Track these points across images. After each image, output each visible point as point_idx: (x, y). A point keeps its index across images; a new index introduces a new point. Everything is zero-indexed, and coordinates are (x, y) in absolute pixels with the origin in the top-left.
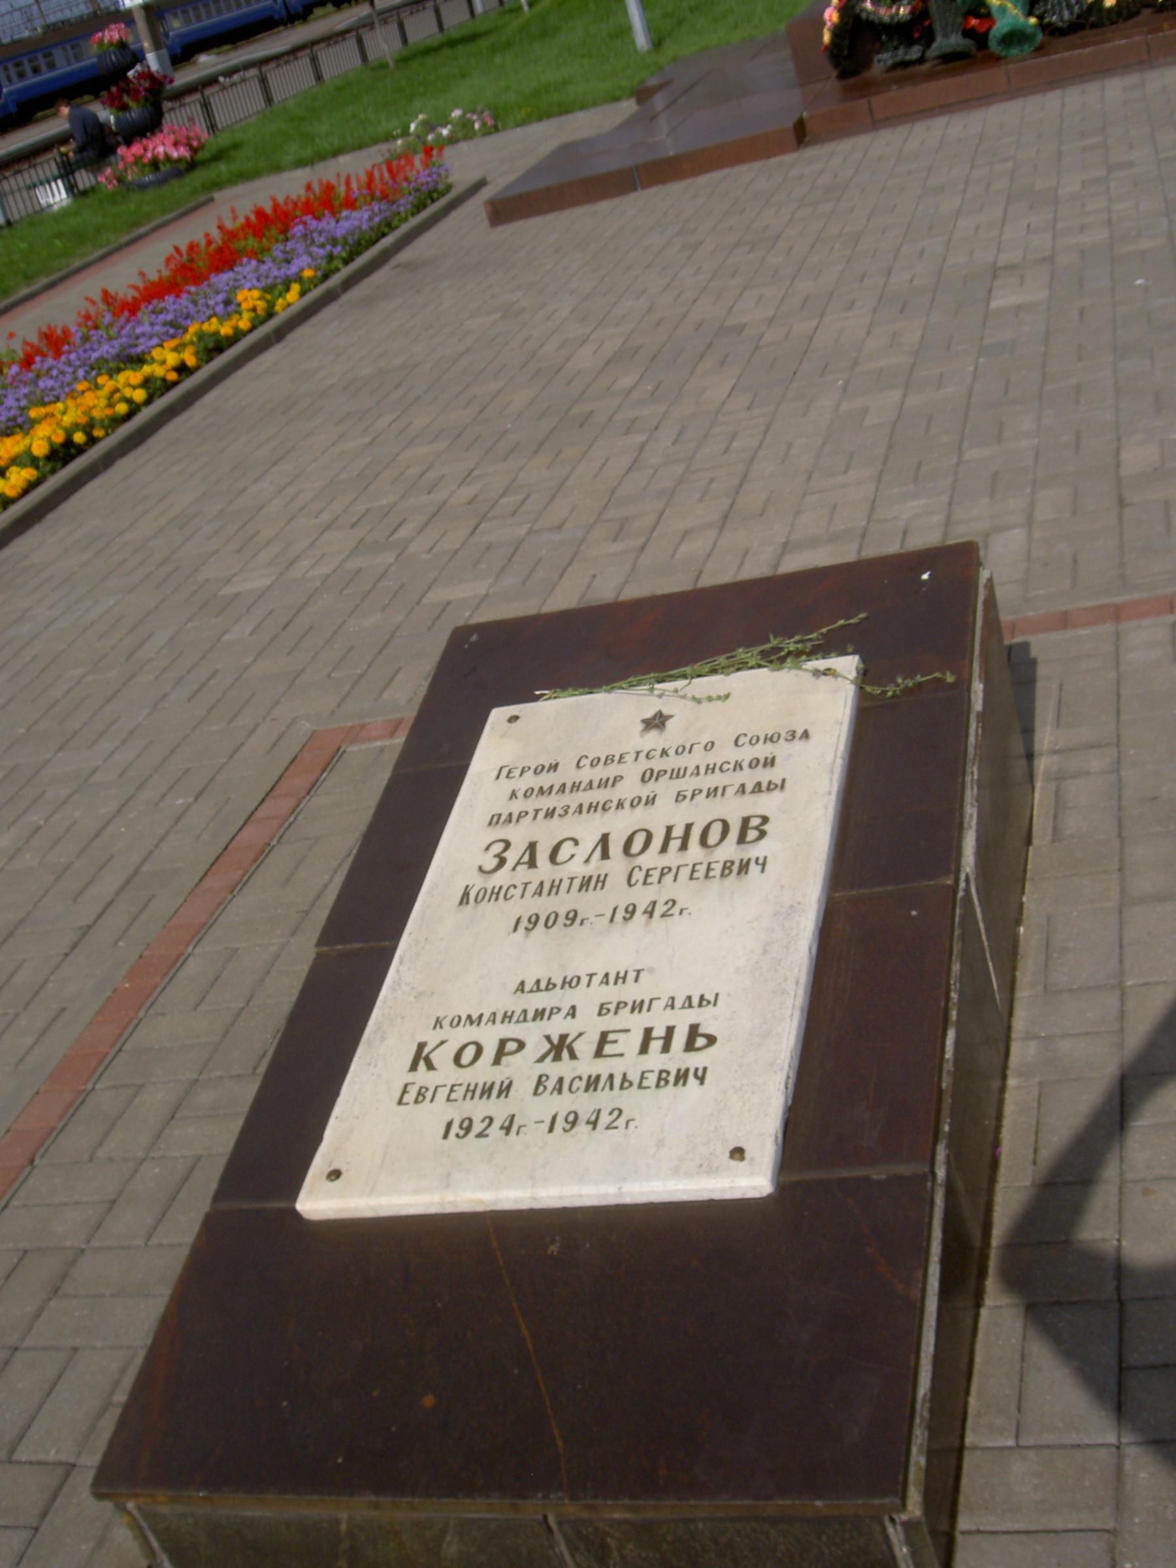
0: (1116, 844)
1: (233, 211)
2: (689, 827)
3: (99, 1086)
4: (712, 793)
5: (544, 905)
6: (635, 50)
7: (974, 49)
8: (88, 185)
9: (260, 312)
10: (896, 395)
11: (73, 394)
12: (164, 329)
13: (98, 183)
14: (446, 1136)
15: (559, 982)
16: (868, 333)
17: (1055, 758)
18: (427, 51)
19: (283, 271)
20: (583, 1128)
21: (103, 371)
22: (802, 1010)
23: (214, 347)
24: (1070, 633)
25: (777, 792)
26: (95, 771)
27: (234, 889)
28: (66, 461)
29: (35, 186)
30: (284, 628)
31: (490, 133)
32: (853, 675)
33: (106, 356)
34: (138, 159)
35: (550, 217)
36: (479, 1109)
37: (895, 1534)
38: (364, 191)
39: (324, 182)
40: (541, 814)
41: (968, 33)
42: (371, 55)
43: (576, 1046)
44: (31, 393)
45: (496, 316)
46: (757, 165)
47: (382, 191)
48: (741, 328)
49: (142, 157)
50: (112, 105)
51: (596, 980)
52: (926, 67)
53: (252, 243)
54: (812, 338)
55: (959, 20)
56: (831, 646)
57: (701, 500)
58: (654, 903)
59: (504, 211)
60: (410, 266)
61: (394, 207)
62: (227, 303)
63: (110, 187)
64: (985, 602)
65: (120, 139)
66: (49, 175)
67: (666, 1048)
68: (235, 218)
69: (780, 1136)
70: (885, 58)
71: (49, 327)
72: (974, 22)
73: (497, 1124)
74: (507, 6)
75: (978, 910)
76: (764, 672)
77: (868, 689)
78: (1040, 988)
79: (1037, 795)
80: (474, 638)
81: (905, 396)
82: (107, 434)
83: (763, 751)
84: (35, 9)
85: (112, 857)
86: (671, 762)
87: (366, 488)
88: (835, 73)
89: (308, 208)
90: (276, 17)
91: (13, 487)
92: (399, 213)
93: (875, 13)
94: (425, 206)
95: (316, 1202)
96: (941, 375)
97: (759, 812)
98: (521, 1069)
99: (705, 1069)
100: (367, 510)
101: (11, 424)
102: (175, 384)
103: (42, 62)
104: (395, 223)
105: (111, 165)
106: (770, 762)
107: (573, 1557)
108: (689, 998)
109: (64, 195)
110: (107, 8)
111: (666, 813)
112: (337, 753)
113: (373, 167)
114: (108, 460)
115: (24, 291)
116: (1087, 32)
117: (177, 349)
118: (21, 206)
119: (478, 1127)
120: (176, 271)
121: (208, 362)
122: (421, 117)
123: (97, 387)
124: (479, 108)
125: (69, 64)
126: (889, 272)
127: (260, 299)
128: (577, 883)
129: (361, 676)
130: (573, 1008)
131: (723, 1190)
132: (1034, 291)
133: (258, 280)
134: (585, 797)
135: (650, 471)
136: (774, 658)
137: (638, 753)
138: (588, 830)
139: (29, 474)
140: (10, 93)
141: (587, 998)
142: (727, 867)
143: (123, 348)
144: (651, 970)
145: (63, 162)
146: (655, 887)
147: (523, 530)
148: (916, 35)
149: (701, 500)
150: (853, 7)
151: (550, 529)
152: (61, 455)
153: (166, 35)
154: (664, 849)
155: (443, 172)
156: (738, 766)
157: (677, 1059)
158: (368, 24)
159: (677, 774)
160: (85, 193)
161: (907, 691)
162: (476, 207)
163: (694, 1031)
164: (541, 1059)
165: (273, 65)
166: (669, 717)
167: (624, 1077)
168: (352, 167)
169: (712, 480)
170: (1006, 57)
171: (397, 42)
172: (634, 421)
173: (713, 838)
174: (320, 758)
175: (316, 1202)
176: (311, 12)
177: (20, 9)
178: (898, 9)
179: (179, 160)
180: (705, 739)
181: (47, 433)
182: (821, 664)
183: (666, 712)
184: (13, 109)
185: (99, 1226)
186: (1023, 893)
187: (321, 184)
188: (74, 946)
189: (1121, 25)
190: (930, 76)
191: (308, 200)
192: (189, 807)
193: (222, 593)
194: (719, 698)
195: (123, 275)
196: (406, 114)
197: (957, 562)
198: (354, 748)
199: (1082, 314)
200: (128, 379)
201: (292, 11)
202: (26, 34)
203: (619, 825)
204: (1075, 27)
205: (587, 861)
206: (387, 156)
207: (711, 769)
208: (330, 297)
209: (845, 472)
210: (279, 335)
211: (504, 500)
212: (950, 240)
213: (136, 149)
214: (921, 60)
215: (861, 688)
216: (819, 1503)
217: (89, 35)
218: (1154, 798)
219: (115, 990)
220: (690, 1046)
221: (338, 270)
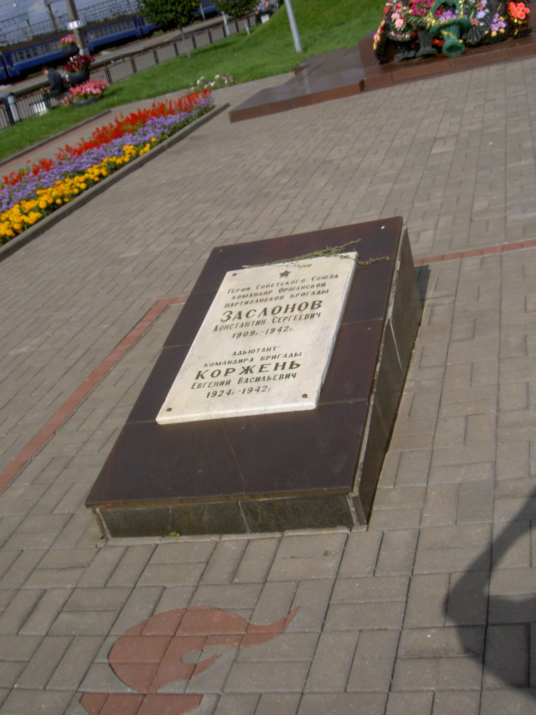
0: (450, 325)
1: (121, 114)
2: (294, 305)
3: (79, 410)
4: (303, 295)
5: (243, 330)
6: (295, 51)
7: (436, 53)
8: (55, 105)
9: (133, 155)
10: (390, 185)
11: (54, 186)
12: (93, 161)
13: (60, 104)
14: (208, 397)
15: (248, 352)
16: (382, 163)
17: (432, 300)
18: (205, 51)
19: (143, 138)
20: (254, 392)
21: (67, 176)
22: (329, 356)
23: (114, 168)
24: (444, 262)
25: (325, 294)
26: (71, 318)
27: (128, 350)
28: (54, 210)
29: (33, 104)
30: (145, 269)
31: (231, 85)
32: (354, 257)
33: (68, 171)
34: (78, 94)
35: (257, 119)
36: (219, 389)
37: (350, 502)
38: (178, 107)
39: (160, 103)
40: (243, 303)
41: (434, 46)
42: (180, 52)
43: (252, 369)
44: (38, 184)
45: (233, 157)
46: (343, 99)
47: (185, 107)
48: (332, 161)
49: (80, 93)
50: (68, 70)
51: (260, 351)
52: (416, 60)
53: (129, 127)
54: (359, 164)
55: (431, 40)
56: (348, 249)
57: (311, 222)
58: (281, 328)
59: (237, 116)
60: (197, 138)
61: (190, 114)
62: (119, 151)
63: (66, 105)
64: (404, 237)
65: (70, 85)
66: (39, 100)
67: (283, 368)
68: (122, 117)
69: (319, 391)
70: (399, 56)
71: (44, 159)
72: (437, 41)
73: (225, 392)
74: (240, 33)
75: (393, 332)
76: (324, 257)
77: (360, 262)
78: (417, 367)
79: (424, 311)
80: (221, 251)
81: (394, 185)
82: (70, 201)
83: (321, 281)
84: (28, 29)
85: (79, 345)
86: (290, 286)
87: (178, 220)
88: (378, 62)
89: (154, 114)
90: (137, 35)
91: (31, 220)
92: (192, 117)
93: (395, 37)
94: (203, 114)
95: (163, 418)
96: (409, 177)
97: (319, 300)
98: (234, 377)
99: (296, 374)
100: (178, 228)
101: (29, 196)
102: (97, 182)
103: (31, 52)
104: (190, 120)
105: (66, 96)
106: (324, 285)
107: (246, 517)
108: (292, 354)
109: (45, 108)
110: (61, 29)
111: (287, 301)
112: (167, 307)
113: (182, 97)
114: (70, 211)
115: (29, 147)
116: (484, 47)
117: (99, 168)
118: (27, 113)
119: (218, 394)
120: (96, 138)
121: (111, 174)
122: (202, 78)
123: (65, 182)
124: (227, 74)
125: (44, 53)
126: (393, 141)
127: (133, 149)
128: (255, 323)
129: (176, 284)
130: (252, 359)
131: (300, 407)
132: (450, 147)
133: (132, 141)
134: (259, 298)
135: (292, 212)
136: (328, 253)
137: (278, 284)
138: (260, 308)
139: (38, 215)
140: (17, 66)
141: (257, 356)
142: (307, 316)
143: (76, 168)
144: (279, 347)
145: (45, 95)
146: (282, 323)
147: (240, 234)
148: (413, 47)
149: (311, 222)
150: (386, 34)
151: (251, 233)
152: (51, 208)
153: (88, 42)
154: (286, 311)
155: (211, 100)
156: (313, 286)
157: (287, 371)
158: (179, 39)
159: (291, 289)
160: (54, 108)
161: (373, 263)
162: (225, 115)
163: (293, 363)
164: (241, 374)
165: (137, 55)
166: (289, 272)
167: (269, 377)
168: (172, 98)
169: (316, 215)
170: (449, 56)
171: (192, 47)
172: (286, 195)
173: (302, 308)
174: (161, 308)
175: (163, 418)
176: (153, 34)
177: (21, 29)
178: (405, 36)
179: (96, 95)
180: (302, 279)
181: (45, 199)
182: (344, 254)
183: (288, 271)
184: (18, 73)
185: (81, 449)
186: (415, 340)
187: (159, 104)
188: (65, 373)
189: (499, 44)
190: (418, 64)
191: (153, 110)
192: (108, 328)
193: (119, 257)
194: (307, 266)
195: (74, 140)
196: (195, 77)
197: (395, 223)
198: (174, 305)
199: (466, 155)
200: (78, 179)
201: (144, 33)
202: (25, 40)
203: (270, 306)
204: (479, 44)
205: (259, 316)
206: (187, 94)
207: (303, 288)
208: (162, 150)
209: (368, 212)
210: (141, 164)
211: (234, 223)
212: (418, 128)
213: (78, 89)
214: (414, 57)
215: (357, 263)
216: (325, 489)
217: (59, 39)
218: (465, 311)
219: (84, 382)
220: (291, 367)
221: (166, 139)
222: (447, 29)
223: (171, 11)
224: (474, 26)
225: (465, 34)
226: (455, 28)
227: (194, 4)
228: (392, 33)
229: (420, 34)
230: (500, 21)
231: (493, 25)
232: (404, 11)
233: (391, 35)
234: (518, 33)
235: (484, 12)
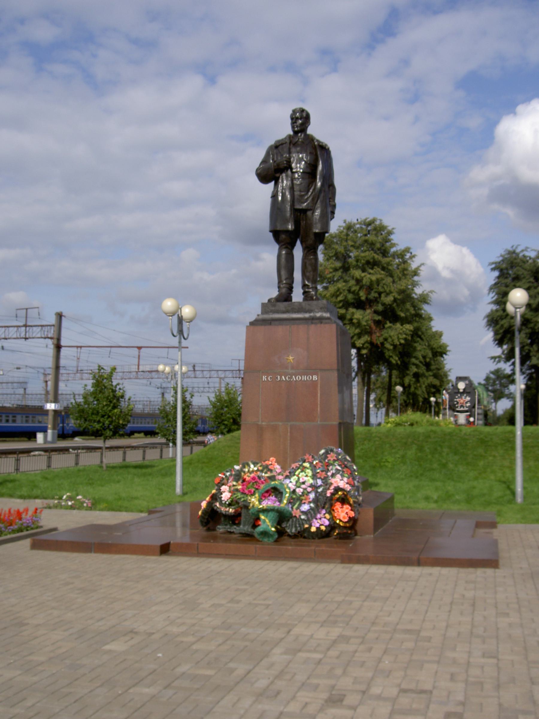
103: (11, 418)
122: (68, 494)
125: (22, 423)
150: (213, 503)
170: (258, 541)
176: (133, 434)
190: (237, 541)
222: (265, 514)
223: (99, 422)
224: (295, 516)
225: (285, 523)
227: (121, 422)
228: (218, 504)
230: (325, 518)
231: (314, 520)
232: (234, 486)
233: (216, 506)
234: (338, 534)
235: (308, 506)
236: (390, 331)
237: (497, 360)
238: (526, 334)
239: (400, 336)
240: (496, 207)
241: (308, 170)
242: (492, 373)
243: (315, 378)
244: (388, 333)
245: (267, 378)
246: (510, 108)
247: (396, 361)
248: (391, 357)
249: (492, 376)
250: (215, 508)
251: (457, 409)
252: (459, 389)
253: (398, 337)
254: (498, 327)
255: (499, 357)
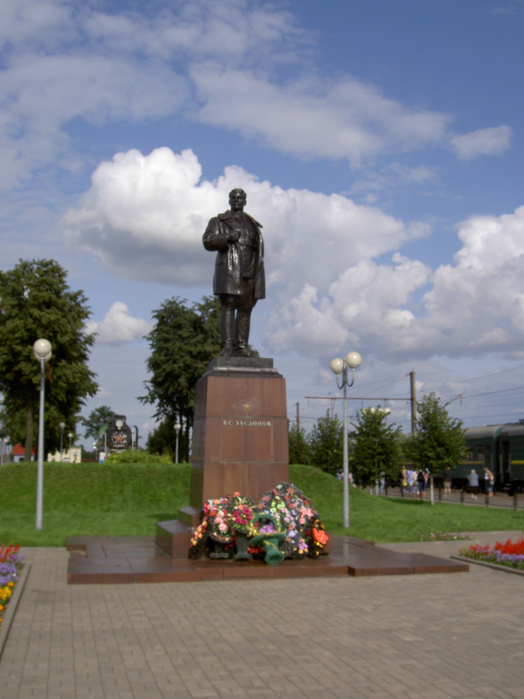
226: (276, 541)
228: (215, 534)
229: (240, 540)
236: (64, 370)
237: (144, 400)
238: (186, 378)
239: (76, 375)
240: (87, 248)
241: (251, 244)
242: (97, 410)
243: (269, 424)
244: (62, 371)
245: (227, 423)
246: (108, 156)
247: (62, 398)
248: (59, 394)
249: (97, 413)
250: (212, 537)
251: (114, 446)
252: (116, 427)
253: (74, 376)
254: (160, 370)
255: (146, 397)
